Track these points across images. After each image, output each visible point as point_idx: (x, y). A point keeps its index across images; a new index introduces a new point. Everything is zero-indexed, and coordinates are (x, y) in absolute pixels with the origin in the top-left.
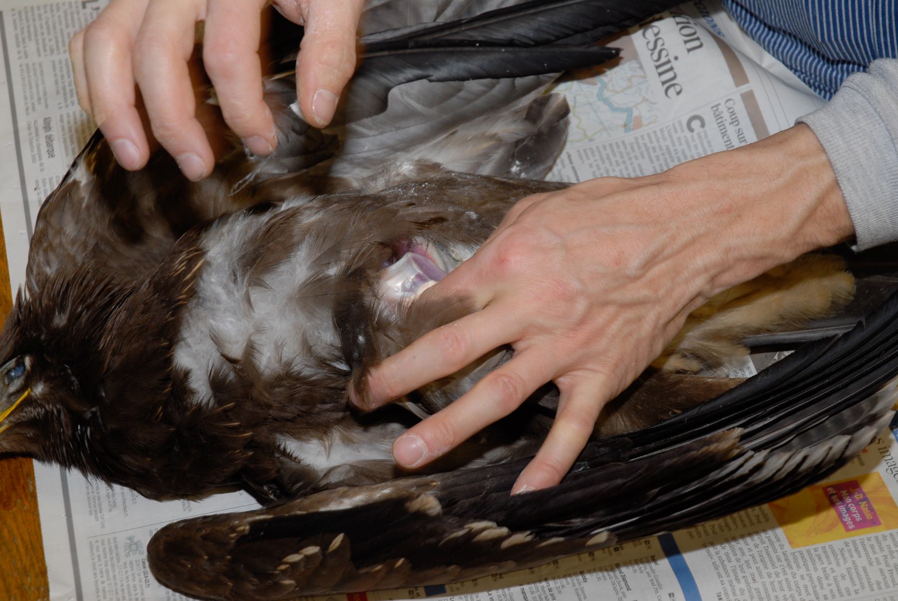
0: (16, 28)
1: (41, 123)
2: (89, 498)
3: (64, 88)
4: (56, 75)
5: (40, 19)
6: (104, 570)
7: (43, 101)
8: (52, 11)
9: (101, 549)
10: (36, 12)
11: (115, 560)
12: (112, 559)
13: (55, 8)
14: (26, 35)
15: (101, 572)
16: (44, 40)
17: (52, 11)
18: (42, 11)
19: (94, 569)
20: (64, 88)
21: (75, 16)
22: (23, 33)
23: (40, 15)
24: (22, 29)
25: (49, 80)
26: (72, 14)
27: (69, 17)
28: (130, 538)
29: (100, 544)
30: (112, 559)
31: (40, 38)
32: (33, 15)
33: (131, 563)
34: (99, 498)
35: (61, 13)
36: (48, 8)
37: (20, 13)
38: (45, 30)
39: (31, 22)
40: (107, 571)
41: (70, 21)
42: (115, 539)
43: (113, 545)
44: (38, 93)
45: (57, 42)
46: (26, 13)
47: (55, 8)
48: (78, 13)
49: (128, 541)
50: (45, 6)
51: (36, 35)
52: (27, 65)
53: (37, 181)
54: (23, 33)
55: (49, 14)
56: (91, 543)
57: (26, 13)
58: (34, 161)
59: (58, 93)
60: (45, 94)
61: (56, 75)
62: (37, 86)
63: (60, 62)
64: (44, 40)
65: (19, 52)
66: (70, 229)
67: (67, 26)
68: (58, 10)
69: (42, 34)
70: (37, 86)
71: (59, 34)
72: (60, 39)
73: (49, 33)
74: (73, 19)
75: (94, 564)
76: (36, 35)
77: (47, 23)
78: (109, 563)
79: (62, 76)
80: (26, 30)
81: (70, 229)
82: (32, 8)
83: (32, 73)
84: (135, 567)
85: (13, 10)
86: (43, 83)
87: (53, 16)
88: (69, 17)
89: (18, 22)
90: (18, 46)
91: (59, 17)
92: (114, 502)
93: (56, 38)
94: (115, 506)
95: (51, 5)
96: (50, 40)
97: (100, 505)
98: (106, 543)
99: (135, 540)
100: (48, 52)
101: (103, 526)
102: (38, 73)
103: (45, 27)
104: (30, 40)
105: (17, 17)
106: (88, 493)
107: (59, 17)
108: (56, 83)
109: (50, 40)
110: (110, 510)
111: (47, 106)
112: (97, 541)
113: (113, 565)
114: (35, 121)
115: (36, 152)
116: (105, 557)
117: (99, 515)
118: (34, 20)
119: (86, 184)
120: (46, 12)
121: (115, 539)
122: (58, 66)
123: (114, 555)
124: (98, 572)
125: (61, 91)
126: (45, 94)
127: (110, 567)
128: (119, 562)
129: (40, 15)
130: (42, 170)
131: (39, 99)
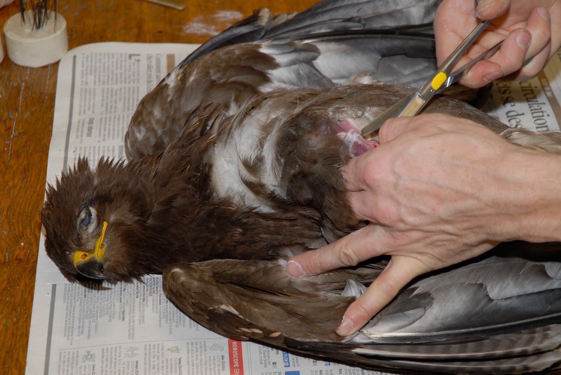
0: (83, 66)
1: (87, 120)
2: (66, 327)
3: (107, 104)
4: (103, 96)
5: (100, 62)
6: (66, 369)
7: (91, 109)
8: (109, 58)
9: (67, 357)
10: (98, 57)
11: (74, 364)
12: (72, 363)
13: (111, 56)
14: (89, 71)
15: (63, 371)
16: (100, 76)
17: (109, 58)
18: (102, 57)
19: (59, 368)
20: (107, 104)
21: (123, 63)
22: (87, 70)
23: (100, 60)
24: (87, 67)
25: (98, 99)
26: (121, 61)
27: (119, 63)
28: (88, 352)
29: (67, 354)
30: (72, 363)
31: (97, 74)
32: (96, 59)
33: (85, 366)
34: (73, 328)
35: (114, 60)
36: (106, 56)
37: (87, 57)
38: (102, 70)
39: (94, 63)
40: (68, 370)
41: (119, 66)
42: (77, 352)
43: (75, 356)
44: (89, 104)
45: (108, 78)
46: (92, 57)
47: (111, 56)
48: (125, 61)
49: (86, 354)
50: (105, 54)
51: (95, 72)
52: (86, 90)
53: (76, 148)
54: (87, 70)
55: (106, 60)
56: (61, 353)
57: (92, 57)
58: (77, 137)
59: (102, 106)
60: (94, 105)
61: (103, 96)
62: (90, 100)
63: (108, 89)
64: (100, 76)
65: (82, 82)
66: (157, 113)
67: (117, 69)
68: (113, 57)
69: (100, 72)
70: (90, 100)
71: (110, 74)
72: (110, 76)
73: (104, 72)
74: (121, 65)
75: (60, 365)
76: (95, 72)
77: (104, 65)
78: (70, 366)
79: (107, 97)
80: (89, 68)
81: (157, 113)
82: (96, 54)
83: (88, 94)
84: (87, 369)
85: (83, 54)
86: (94, 99)
87: (109, 61)
88: (119, 63)
89: (85, 63)
90: (82, 77)
91: (113, 62)
92: (82, 331)
93: (108, 76)
94: (82, 333)
95: (109, 54)
96: (104, 76)
97: (72, 332)
98: (71, 354)
99: (91, 353)
100: (101, 83)
101: (71, 344)
102: (92, 94)
103: (102, 67)
104: (91, 74)
105: (85, 59)
106: (66, 324)
107: (113, 62)
108: (103, 100)
109: (104, 76)
110: (79, 336)
111: (93, 112)
112: (65, 352)
113: (72, 367)
114: (84, 120)
115: (80, 133)
116: (68, 362)
117: (70, 337)
118: (96, 62)
119: (174, 87)
120: (104, 58)
121: (77, 352)
122: (105, 91)
123: (75, 361)
124: (61, 370)
125: (105, 105)
126: (94, 105)
127: (70, 368)
128: (77, 365)
129: (100, 60)
130: (81, 143)
131: (89, 108)
